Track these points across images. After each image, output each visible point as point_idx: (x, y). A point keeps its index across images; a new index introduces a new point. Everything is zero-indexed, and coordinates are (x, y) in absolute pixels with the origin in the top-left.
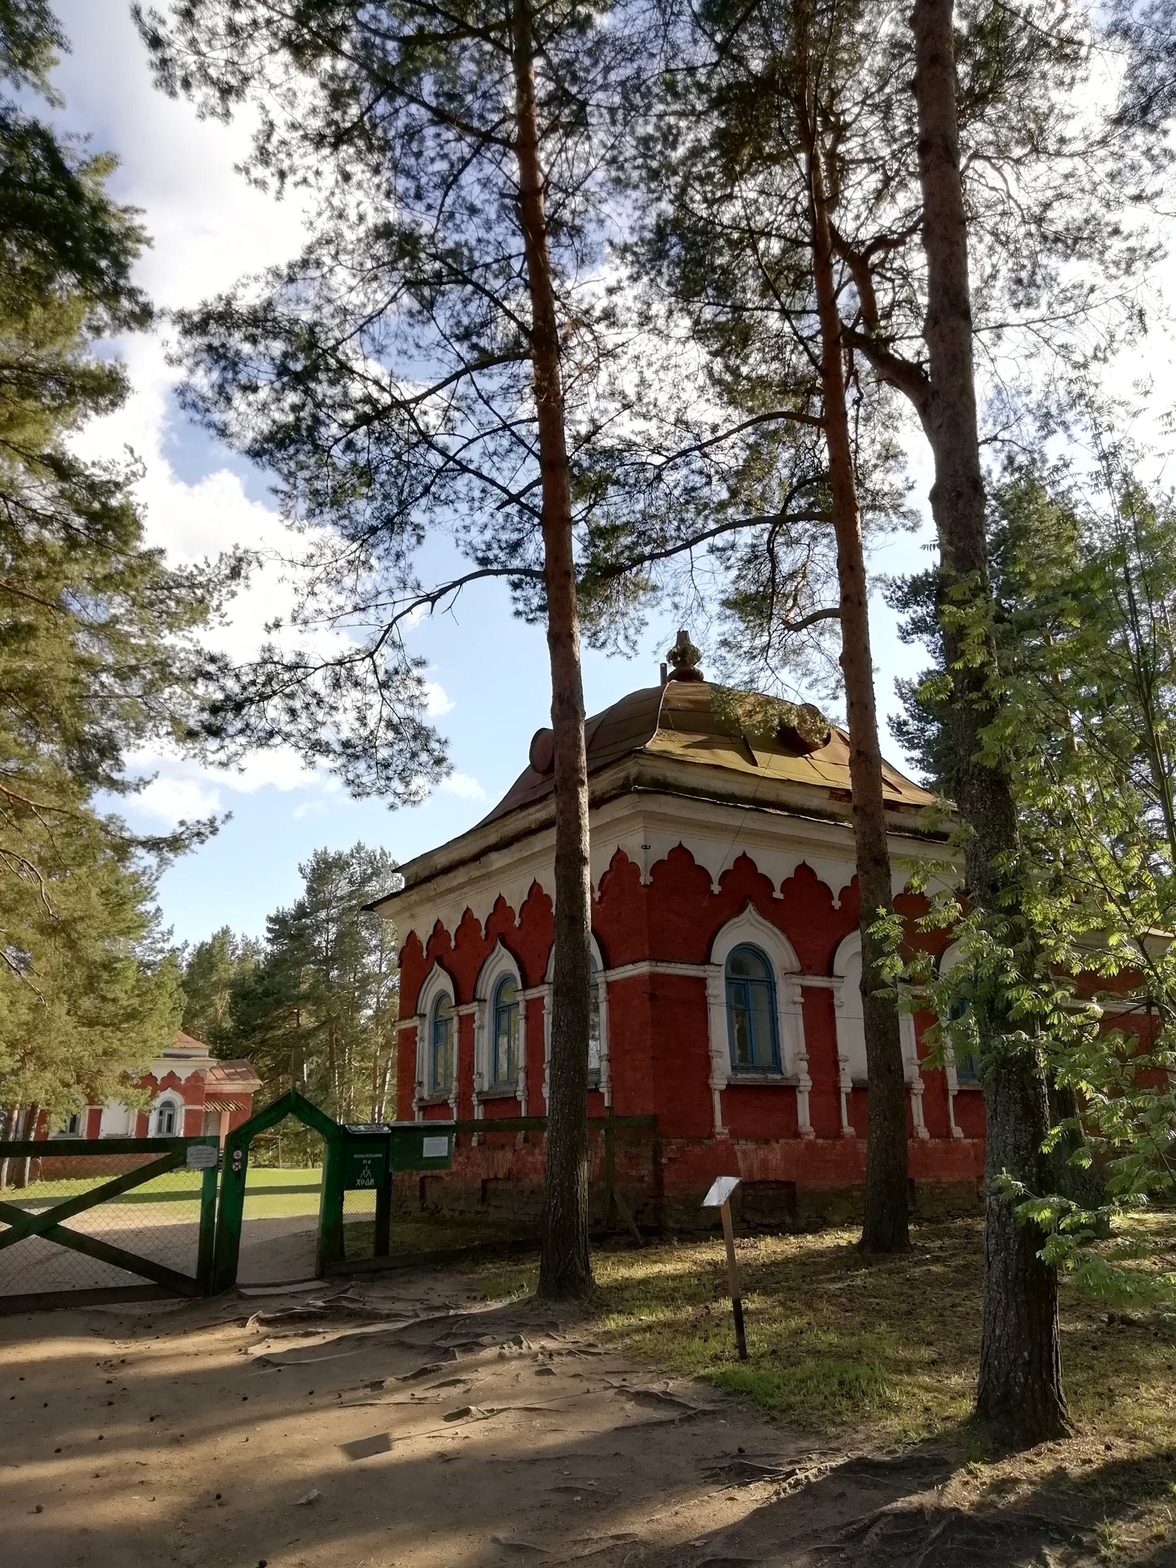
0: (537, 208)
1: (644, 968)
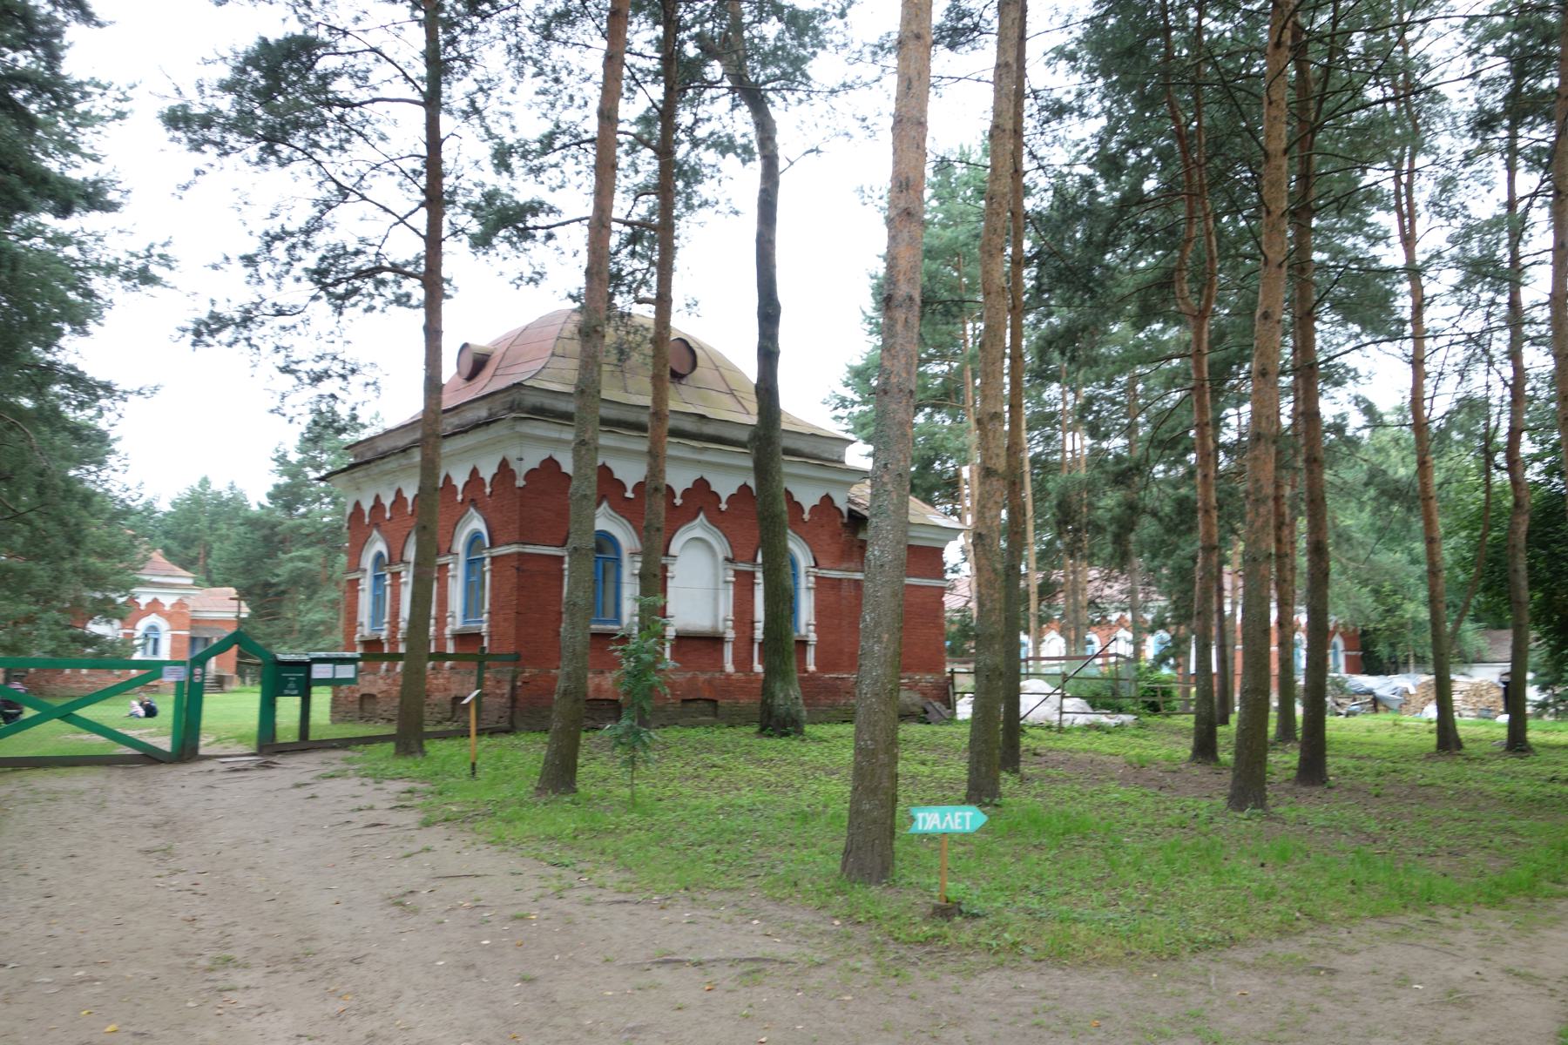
0: (665, 32)
1: (514, 549)
